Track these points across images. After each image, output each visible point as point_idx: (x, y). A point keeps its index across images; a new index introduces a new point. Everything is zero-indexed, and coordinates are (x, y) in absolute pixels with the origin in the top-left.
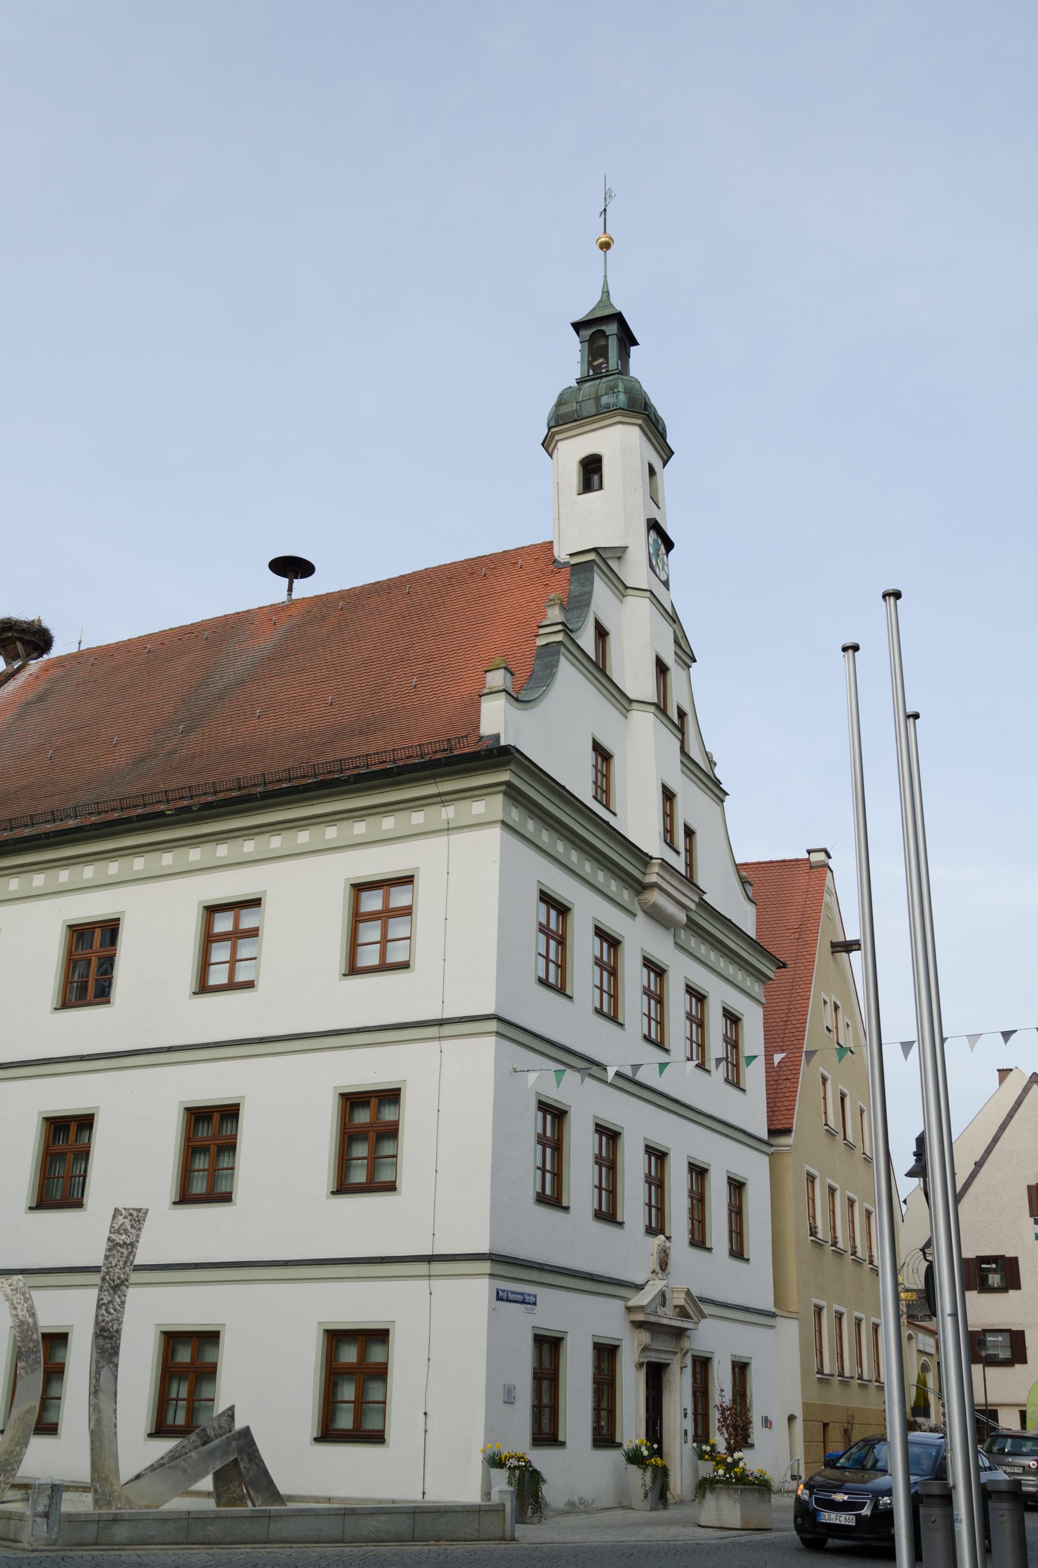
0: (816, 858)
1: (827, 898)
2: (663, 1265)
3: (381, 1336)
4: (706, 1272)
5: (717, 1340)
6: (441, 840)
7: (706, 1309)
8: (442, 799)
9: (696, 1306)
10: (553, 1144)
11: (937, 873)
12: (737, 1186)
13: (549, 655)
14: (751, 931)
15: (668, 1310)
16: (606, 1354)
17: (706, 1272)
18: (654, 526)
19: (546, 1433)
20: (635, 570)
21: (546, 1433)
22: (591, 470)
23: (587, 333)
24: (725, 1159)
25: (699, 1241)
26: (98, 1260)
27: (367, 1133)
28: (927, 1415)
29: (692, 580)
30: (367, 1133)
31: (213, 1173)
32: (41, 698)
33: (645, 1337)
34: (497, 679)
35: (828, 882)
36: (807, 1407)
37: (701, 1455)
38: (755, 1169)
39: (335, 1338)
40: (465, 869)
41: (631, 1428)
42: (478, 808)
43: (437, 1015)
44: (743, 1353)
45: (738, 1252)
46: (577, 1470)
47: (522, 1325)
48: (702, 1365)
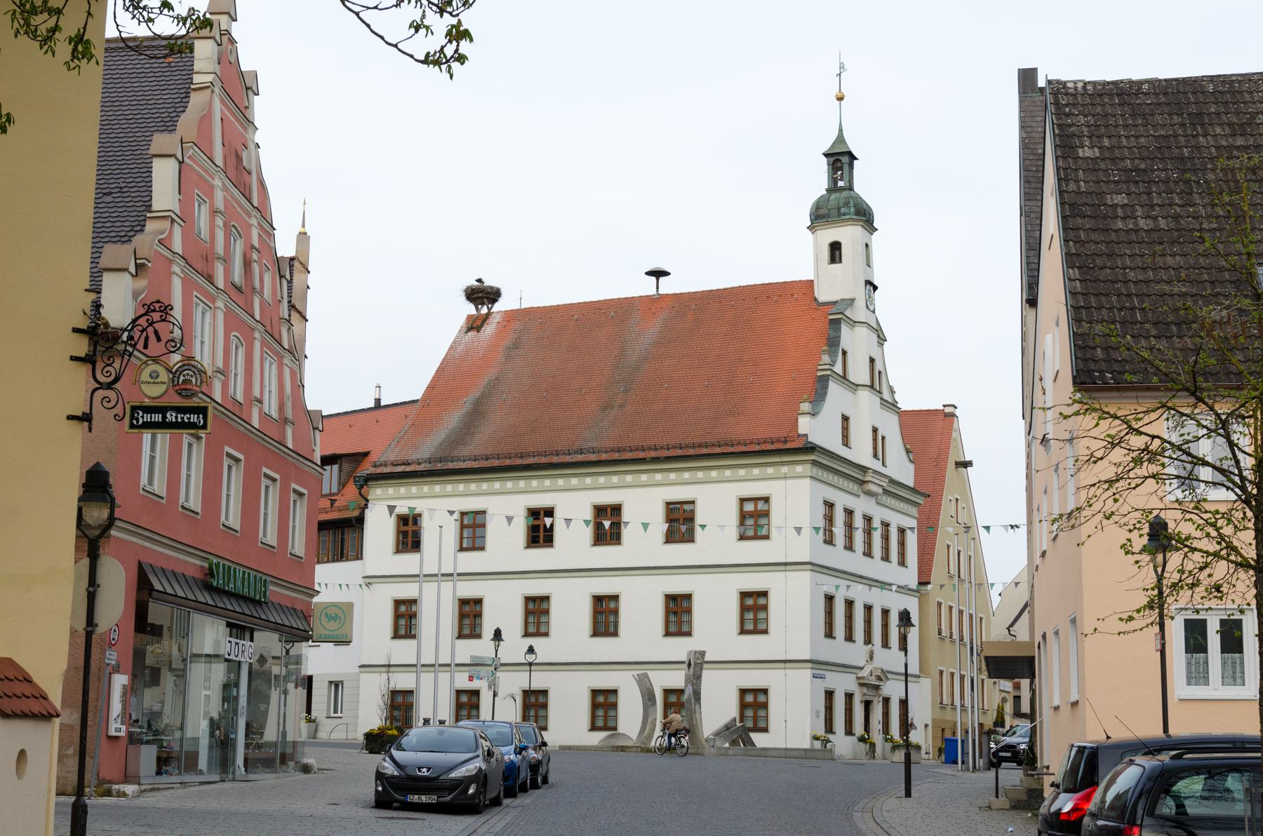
0: (948, 410)
1: (954, 435)
2: (871, 658)
4: (891, 659)
5: (894, 689)
6: (782, 482)
7: (889, 676)
8: (783, 464)
9: (883, 676)
10: (829, 613)
13: (824, 381)
15: (873, 678)
16: (849, 697)
19: (829, 728)
20: (859, 313)
21: (829, 728)
22: (835, 250)
23: (832, 159)
26: (684, 658)
27: (753, 610)
28: (1003, 726)
29: (886, 307)
30: (753, 610)
32: (516, 346)
33: (865, 690)
34: (805, 407)
35: (955, 426)
36: (933, 720)
37: (886, 740)
38: (912, 605)
39: (595, 693)
40: (794, 496)
41: (859, 728)
42: (799, 468)
46: (843, 744)
48: (886, 701)
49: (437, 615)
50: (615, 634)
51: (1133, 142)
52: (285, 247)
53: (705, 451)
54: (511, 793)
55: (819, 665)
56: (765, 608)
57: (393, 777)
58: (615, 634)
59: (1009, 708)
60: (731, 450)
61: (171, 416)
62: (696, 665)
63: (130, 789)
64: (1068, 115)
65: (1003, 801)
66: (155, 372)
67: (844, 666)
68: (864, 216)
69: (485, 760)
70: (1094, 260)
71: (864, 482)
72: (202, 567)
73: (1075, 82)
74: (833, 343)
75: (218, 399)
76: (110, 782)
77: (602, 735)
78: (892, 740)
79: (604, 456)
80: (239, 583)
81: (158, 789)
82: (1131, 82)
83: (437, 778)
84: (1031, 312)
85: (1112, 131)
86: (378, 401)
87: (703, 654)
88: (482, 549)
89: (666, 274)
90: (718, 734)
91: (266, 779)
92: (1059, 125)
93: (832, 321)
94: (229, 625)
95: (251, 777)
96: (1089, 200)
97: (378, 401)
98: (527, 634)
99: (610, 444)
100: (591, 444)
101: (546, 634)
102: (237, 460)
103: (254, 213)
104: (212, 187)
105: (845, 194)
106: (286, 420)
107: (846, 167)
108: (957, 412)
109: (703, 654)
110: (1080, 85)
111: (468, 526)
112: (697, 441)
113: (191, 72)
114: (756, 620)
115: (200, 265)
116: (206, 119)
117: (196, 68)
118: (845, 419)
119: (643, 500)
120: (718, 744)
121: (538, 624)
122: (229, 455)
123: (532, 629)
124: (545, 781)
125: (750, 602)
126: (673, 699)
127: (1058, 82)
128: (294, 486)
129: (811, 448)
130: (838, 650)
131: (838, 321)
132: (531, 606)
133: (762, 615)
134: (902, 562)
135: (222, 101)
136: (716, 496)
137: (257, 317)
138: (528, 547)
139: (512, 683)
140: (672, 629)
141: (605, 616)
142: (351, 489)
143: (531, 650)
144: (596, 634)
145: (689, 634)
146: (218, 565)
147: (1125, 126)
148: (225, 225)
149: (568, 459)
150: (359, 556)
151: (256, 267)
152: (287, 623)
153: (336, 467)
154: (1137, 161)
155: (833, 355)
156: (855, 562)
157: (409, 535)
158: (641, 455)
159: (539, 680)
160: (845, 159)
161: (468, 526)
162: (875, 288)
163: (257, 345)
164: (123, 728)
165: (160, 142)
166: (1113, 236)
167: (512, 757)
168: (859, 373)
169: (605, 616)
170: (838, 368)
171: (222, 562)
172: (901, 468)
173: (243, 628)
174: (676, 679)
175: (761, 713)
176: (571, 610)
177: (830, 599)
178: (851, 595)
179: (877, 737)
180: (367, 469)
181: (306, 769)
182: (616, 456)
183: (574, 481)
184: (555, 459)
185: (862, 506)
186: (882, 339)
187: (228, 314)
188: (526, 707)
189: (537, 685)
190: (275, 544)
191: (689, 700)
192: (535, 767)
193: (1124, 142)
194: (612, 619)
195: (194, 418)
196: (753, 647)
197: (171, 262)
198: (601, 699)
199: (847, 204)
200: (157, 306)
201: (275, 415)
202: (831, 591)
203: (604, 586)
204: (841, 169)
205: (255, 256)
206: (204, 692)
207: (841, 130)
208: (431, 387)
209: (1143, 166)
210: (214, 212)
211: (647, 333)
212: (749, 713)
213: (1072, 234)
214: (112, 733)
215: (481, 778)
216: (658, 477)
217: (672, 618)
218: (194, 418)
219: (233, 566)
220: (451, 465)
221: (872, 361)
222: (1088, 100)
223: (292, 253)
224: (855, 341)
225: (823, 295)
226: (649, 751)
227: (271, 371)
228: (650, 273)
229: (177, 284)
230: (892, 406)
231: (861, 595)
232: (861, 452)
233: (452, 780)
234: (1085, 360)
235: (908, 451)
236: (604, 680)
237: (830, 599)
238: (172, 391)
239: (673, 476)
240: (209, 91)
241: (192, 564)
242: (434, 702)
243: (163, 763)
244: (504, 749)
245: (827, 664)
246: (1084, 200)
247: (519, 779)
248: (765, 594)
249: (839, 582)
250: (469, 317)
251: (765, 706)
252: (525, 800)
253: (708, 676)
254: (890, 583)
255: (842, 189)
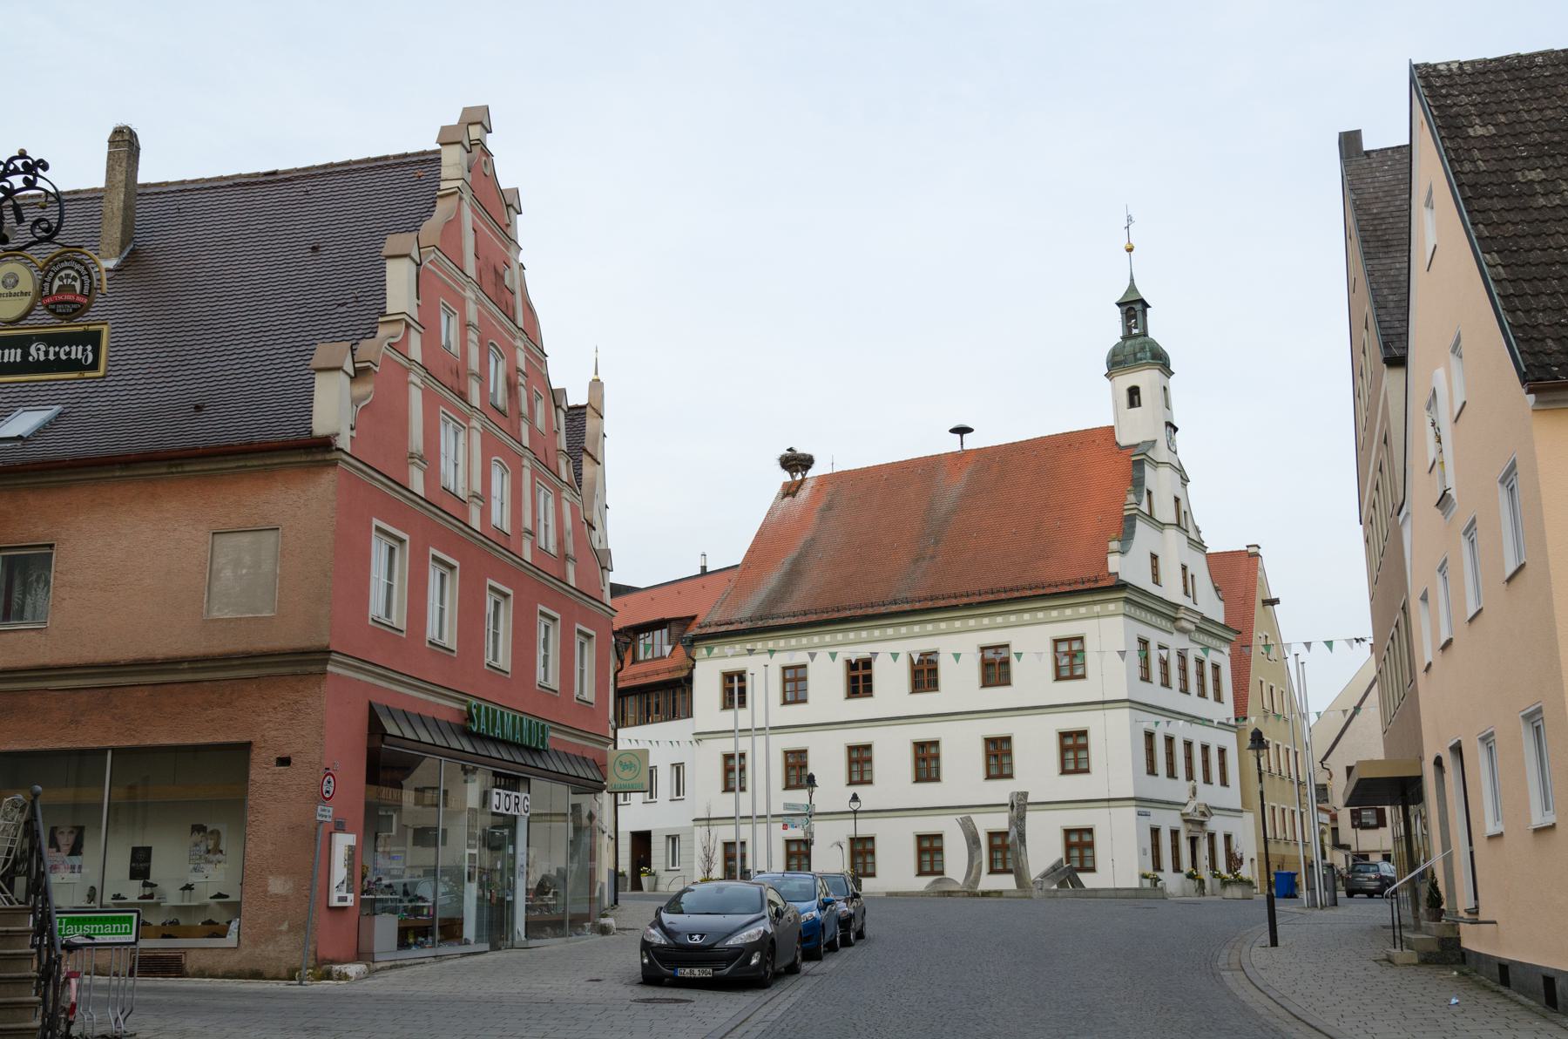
0: (1251, 550)
2: (1194, 794)
3: (1090, 831)
4: (1211, 794)
5: (1217, 825)
6: (1095, 621)
8: (1095, 603)
9: (1208, 811)
10: (1150, 750)
11: (1279, 928)
12: (1222, 751)
13: (1130, 521)
14: (1220, 618)
16: (1175, 834)
17: (1211, 794)
18: (1169, 424)
19: (1157, 866)
20: (1161, 453)
21: (1157, 866)
22: (1134, 394)
24: (1216, 739)
25: (1207, 780)
26: (1007, 801)
29: (1187, 448)
31: (1000, 766)
34: (1114, 545)
40: (1107, 633)
41: (1186, 865)
42: (1112, 607)
43: (1101, 699)
44: (1229, 831)
45: (1224, 783)
46: (1172, 882)
47: (1147, 823)
48: (1212, 836)
49: (766, 767)
50: (937, 779)
51: (1536, 116)
52: (577, 397)
53: (1016, 594)
54: (812, 955)
55: (1143, 803)
56: (1085, 747)
57: (660, 946)
58: (937, 779)
59: (1328, 839)
60: (1042, 592)
61: (37, 352)
62: (1019, 806)
63: (353, 969)
64: (1445, 96)
65: (1408, 955)
66: (13, 275)
67: (1168, 803)
68: (1160, 360)
69: (773, 922)
70: (1516, 243)
71: (1177, 619)
72: (460, 711)
73: (1448, 64)
74: (1138, 483)
75: (573, 583)
76: (333, 962)
77: (931, 879)
78: (1219, 876)
79: (917, 606)
80: (483, 727)
81: (401, 966)
82: (1519, 56)
83: (712, 946)
84: (1392, 378)
85: (1507, 107)
86: (704, 568)
87: (1025, 795)
88: (805, 701)
89: (969, 430)
90: (1045, 876)
91: (552, 945)
92: (1437, 107)
93: (1136, 462)
94: (495, 774)
95: (533, 943)
96: (1494, 179)
97: (704, 568)
98: (851, 783)
99: (923, 594)
100: (904, 595)
101: (870, 782)
102: (589, 637)
103: (519, 334)
104: (464, 299)
105: (1141, 340)
106: (567, 557)
107: (1139, 315)
108: (1261, 552)
109: (1025, 795)
110: (1454, 67)
111: (790, 681)
112: (1009, 585)
113: (438, 179)
114: (1076, 760)
115: (448, 379)
116: (453, 224)
117: (443, 175)
118: (1154, 557)
119: (959, 645)
120: (1046, 886)
121: (862, 772)
122: (580, 632)
123: (856, 778)
124: (860, 935)
125: (1069, 742)
126: (998, 841)
127: (1426, 65)
128: (578, 626)
129: (1123, 586)
130: (1162, 787)
131: (1141, 462)
132: (855, 755)
133: (1082, 755)
134: (1218, 698)
135: (474, 211)
136: (1030, 638)
137: (526, 442)
138: (849, 697)
139: (844, 830)
140: (994, 772)
141: (926, 761)
142: (680, 650)
143: (855, 798)
144: (918, 779)
145: (1010, 776)
146: (478, 708)
147: (1523, 101)
148: (481, 341)
149: (883, 610)
150: (689, 714)
151: (523, 393)
152: (572, 772)
153: (665, 631)
154: (1547, 135)
155: (1138, 494)
156: (1171, 698)
157: (734, 690)
158: (954, 602)
159: (865, 828)
160: (1138, 307)
161: (790, 681)
162: (1176, 429)
163: (527, 474)
164: (351, 896)
165: (393, 243)
166: (1536, 215)
167: (815, 913)
168: (1165, 513)
169: (926, 761)
170: (1144, 507)
171: (484, 705)
172: (1215, 610)
173: (518, 778)
174: (1000, 822)
175: (1088, 853)
176: (893, 757)
177: (1150, 736)
178: (1170, 731)
179: (1205, 874)
180: (694, 631)
181: (604, 930)
182: (930, 604)
183: (890, 631)
184: (870, 611)
185: (1176, 642)
186: (1185, 480)
187: (486, 436)
188: (854, 854)
189: (862, 833)
190: (557, 688)
191: (1014, 842)
192: (845, 922)
193: (1526, 116)
194: (933, 764)
195: (76, 352)
196: (1076, 786)
197: (408, 370)
198: (859, 847)
199: (1142, 349)
200: (19, 163)
201: (552, 550)
202: (1151, 727)
203: (925, 732)
204: (1135, 317)
205: (521, 380)
206: (468, 851)
207: (1132, 280)
208: (751, 551)
209: (1557, 139)
210: (465, 326)
211: (953, 487)
212: (1075, 853)
213: (1480, 217)
214: (334, 902)
215: (767, 945)
216: (972, 622)
217: (993, 761)
218: (76, 352)
219: (499, 709)
220: (771, 623)
221: (1177, 500)
222: (1468, 79)
223: (583, 401)
224: (1156, 479)
225: (1124, 439)
226: (975, 895)
227: (546, 503)
228: (954, 431)
229: (416, 398)
230: (1199, 545)
231: (1181, 731)
232: (1171, 590)
233: (730, 948)
234: (1534, 354)
235: (1217, 590)
236: (929, 825)
237: (1150, 736)
238: (40, 311)
239: (986, 621)
240: (456, 197)
241: (448, 708)
242: (766, 856)
243: (406, 937)
244: (802, 906)
245: (1151, 801)
246: (1487, 179)
247: (825, 937)
248: (1084, 733)
249: (1158, 718)
250: (785, 484)
251: (1091, 845)
252: (830, 964)
253: (1032, 817)
254: (1208, 720)
255: (1137, 336)
